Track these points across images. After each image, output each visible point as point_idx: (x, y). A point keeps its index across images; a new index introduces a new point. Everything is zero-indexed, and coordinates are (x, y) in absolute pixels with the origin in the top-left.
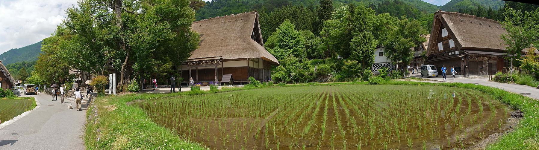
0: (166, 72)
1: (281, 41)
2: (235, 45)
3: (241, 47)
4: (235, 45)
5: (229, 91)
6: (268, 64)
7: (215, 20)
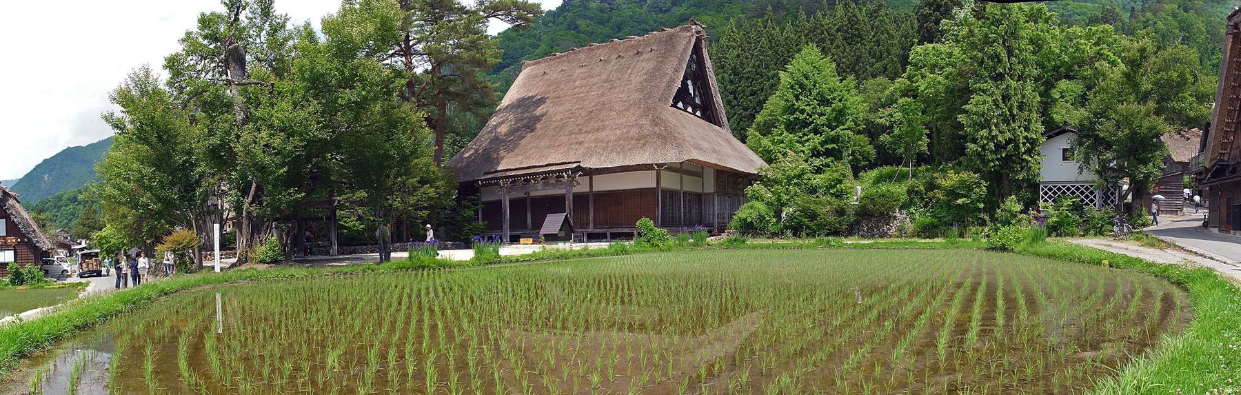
0: (426, 208)
1: (791, 109)
2: (619, 127)
3: (634, 132)
4: (619, 127)
5: (564, 256)
6: (733, 183)
7: (582, 56)
